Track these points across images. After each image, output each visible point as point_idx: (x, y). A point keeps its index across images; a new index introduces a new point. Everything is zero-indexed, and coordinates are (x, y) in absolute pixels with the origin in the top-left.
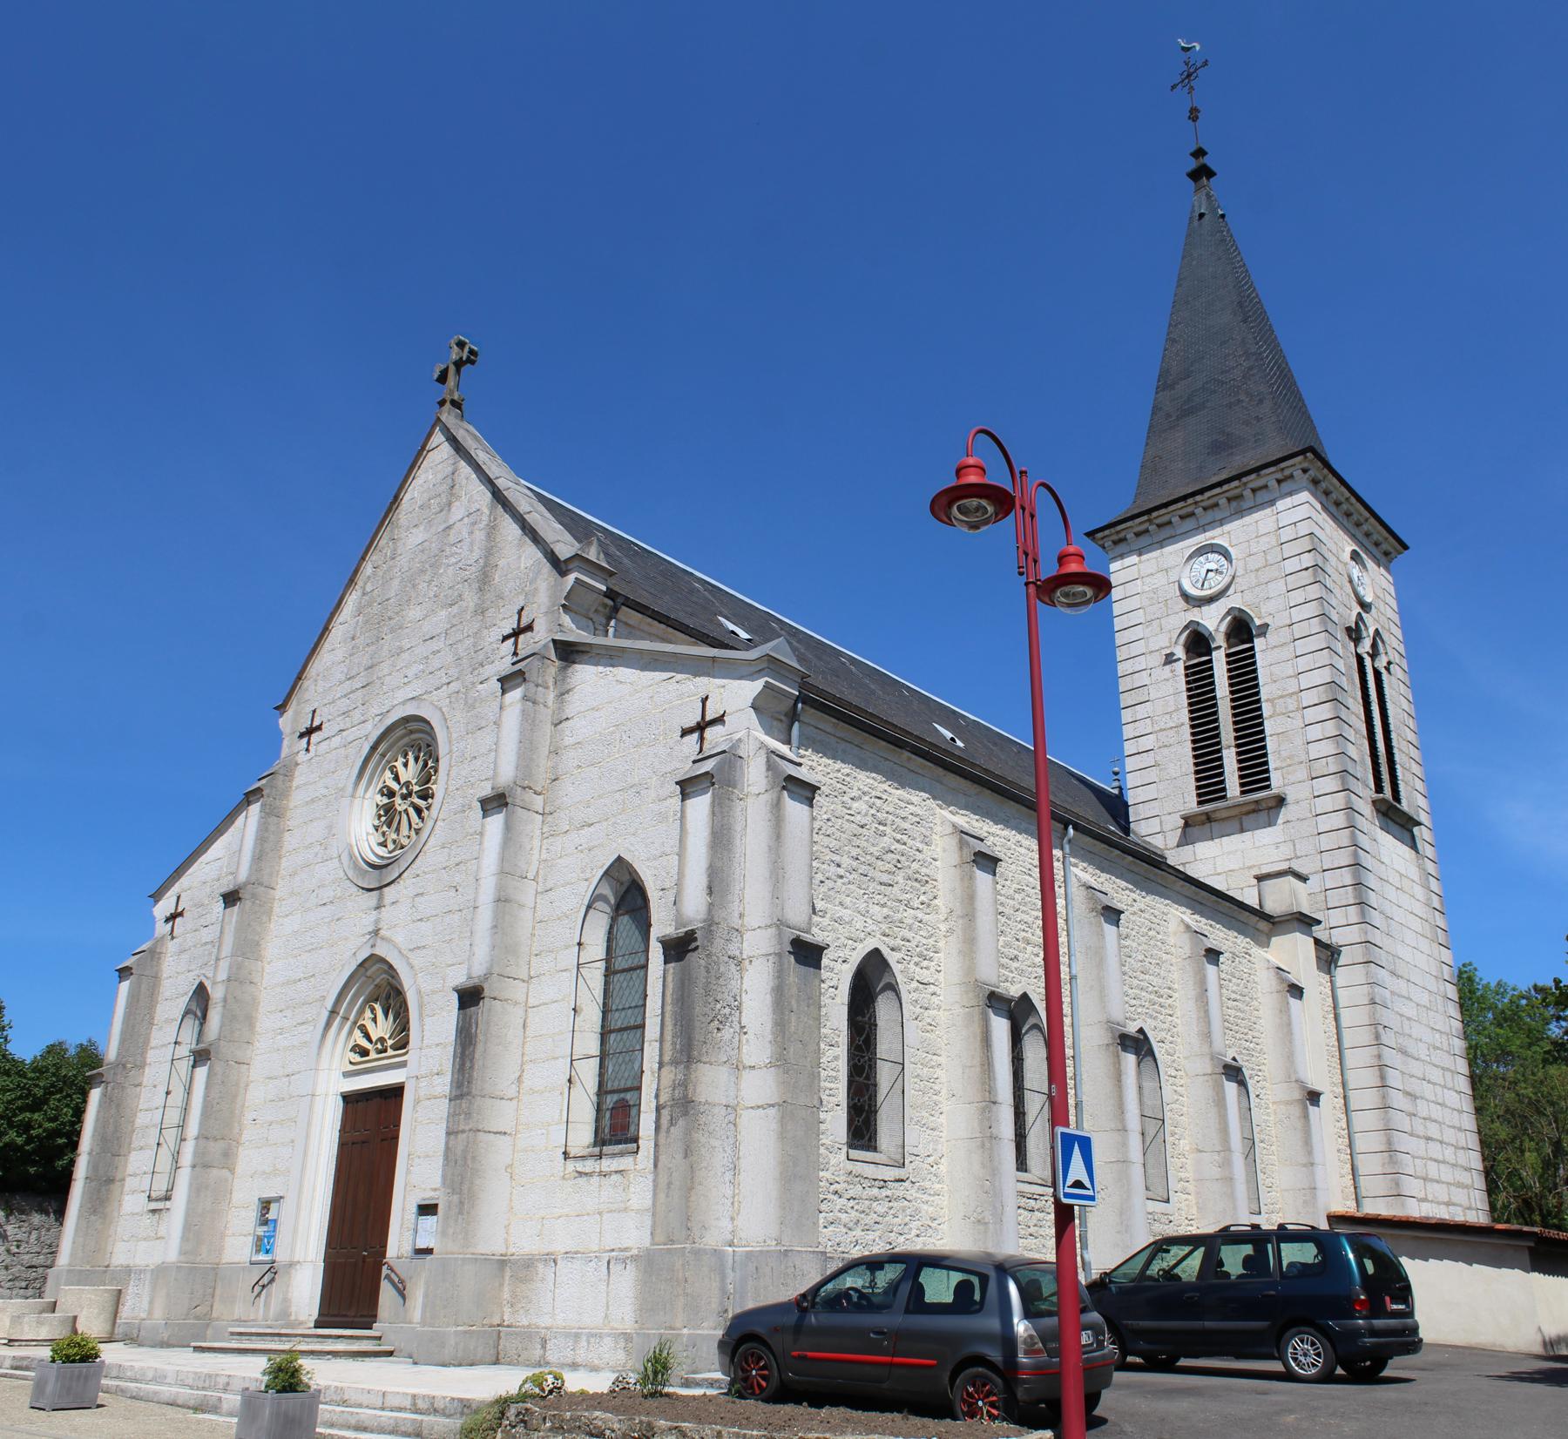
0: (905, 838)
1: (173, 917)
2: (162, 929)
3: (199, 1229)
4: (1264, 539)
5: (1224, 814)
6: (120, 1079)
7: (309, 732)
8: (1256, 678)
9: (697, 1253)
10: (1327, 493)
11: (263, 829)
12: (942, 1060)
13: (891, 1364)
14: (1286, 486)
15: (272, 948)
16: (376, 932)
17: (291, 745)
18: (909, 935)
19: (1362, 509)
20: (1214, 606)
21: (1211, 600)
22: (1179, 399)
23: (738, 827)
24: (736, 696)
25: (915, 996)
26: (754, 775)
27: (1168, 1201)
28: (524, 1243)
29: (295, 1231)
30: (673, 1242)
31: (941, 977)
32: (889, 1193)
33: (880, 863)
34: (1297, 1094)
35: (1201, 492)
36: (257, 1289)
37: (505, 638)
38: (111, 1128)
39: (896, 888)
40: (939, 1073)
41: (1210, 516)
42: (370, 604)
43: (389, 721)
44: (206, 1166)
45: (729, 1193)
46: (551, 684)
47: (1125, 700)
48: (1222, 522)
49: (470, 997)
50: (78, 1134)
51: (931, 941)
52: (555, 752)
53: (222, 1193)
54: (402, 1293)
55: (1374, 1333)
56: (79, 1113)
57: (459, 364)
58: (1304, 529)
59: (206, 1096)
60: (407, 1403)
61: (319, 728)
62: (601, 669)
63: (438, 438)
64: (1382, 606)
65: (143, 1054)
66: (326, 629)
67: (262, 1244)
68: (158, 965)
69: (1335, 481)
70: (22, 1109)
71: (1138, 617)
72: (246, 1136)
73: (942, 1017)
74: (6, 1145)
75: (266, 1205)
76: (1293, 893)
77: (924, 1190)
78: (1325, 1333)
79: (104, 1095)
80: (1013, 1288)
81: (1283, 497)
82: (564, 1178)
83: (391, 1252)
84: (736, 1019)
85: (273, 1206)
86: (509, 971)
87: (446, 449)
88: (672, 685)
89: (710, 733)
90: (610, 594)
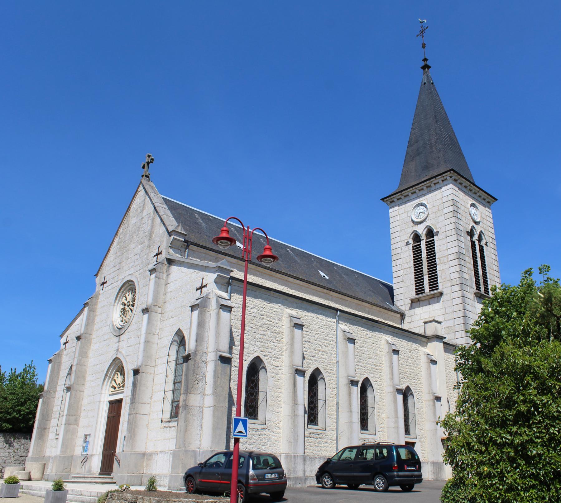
0: (271, 319)
1: (65, 343)
2: (63, 347)
3: (67, 444)
4: (438, 201)
5: (424, 299)
6: (48, 396)
7: (103, 284)
8: (434, 250)
9: (186, 451)
10: (461, 184)
11: (89, 315)
12: (282, 390)
13: (220, 483)
14: (445, 182)
15: (91, 354)
16: (118, 350)
17: (98, 288)
18: (271, 351)
19: (476, 188)
20: (422, 225)
21: (421, 223)
22: (416, 151)
24: (210, 278)
25: (272, 370)
26: (213, 304)
27: (375, 435)
28: (150, 448)
30: (180, 448)
31: (283, 364)
32: (259, 433)
34: (432, 398)
35: (417, 184)
36: (82, 463)
37: (155, 256)
40: (281, 394)
41: (421, 193)
42: (121, 242)
43: (124, 281)
44: (69, 424)
45: (199, 433)
46: (165, 272)
47: (394, 258)
48: (425, 195)
49: (136, 372)
50: (36, 413)
51: (280, 352)
52: (165, 294)
54: (119, 463)
55: (399, 476)
56: (36, 407)
57: (148, 163)
58: (450, 197)
59: (69, 402)
60: (96, 495)
61: (106, 283)
62: (178, 267)
63: (141, 188)
64: (485, 222)
65: (56, 388)
66: (109, 250)
67: (84, 449)
68: (61, 359)
69: (464, 180)
70: (18, 405)
71: (398, 229)
72: (83, 414)
73: (283, 376)
74: (13, 417)
75: (86, 436)
76: (435, 328)
77: (273, 432)
78: (385, 476)
79: (43, 401)
80: (251, 462)
81: (444, 186)
83: (117, 451)
84: (204, 380)
85: (88, 437)
87: (143, 192)
88: (195, 274)
89: (203, 289)
90: (185, 241)
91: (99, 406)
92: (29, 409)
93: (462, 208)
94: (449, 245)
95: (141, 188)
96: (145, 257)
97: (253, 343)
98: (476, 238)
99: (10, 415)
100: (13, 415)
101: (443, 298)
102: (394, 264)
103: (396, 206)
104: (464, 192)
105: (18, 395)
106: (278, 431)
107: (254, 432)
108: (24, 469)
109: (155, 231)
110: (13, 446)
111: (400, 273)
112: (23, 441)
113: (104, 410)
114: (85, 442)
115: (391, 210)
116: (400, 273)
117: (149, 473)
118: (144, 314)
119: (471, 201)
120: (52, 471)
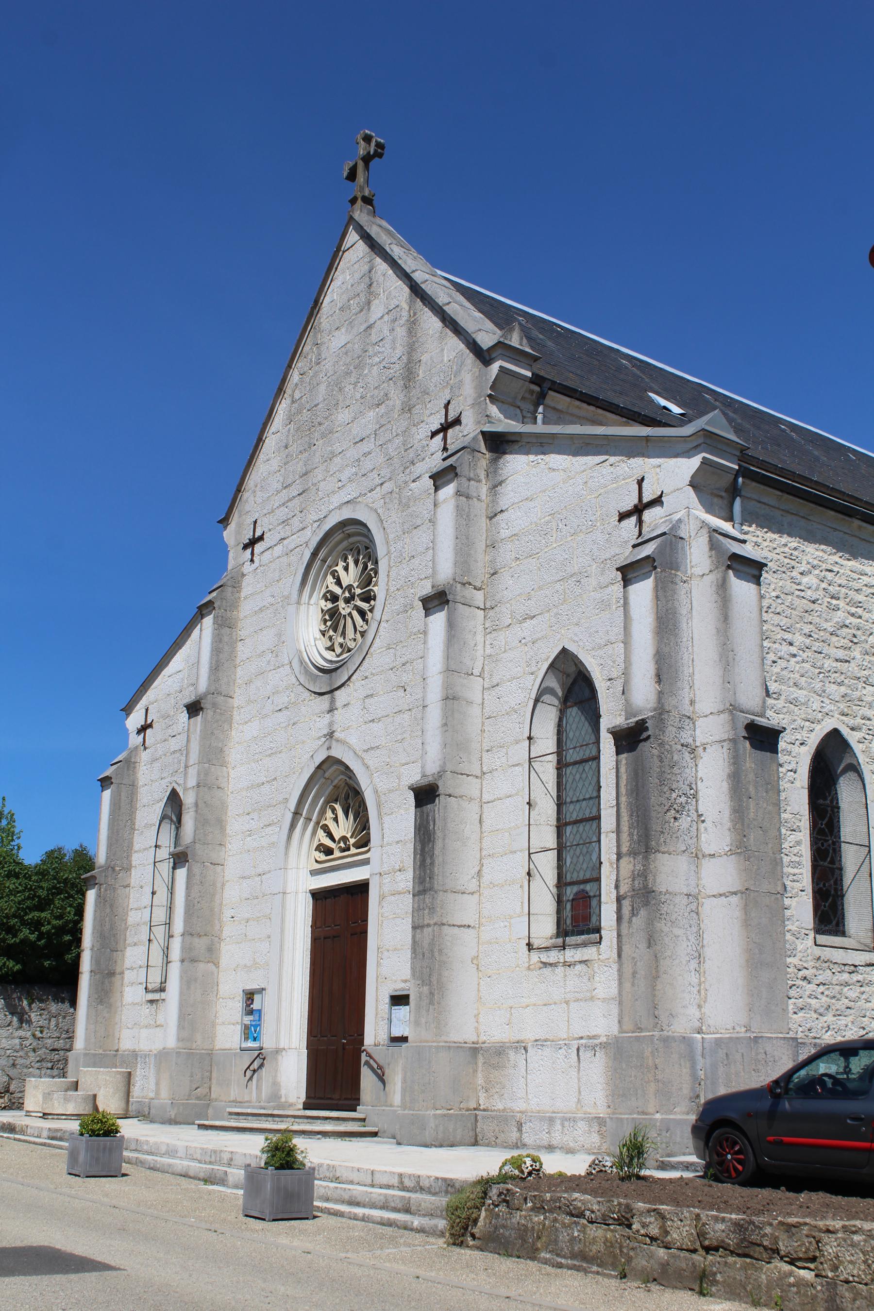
0: (860, 611)
1: (143, 729)
2: (135, 740)
6: (111, 881)
7: (252, 542)
9: (666, 1040)
15: (234, 754)
16: (331, 735)
17: (236, 557)
23: (684, 611)
26: (697, 556)
28: (494, 1032)
29: (278, 1020)
30: (641, 1030)
33: (834, 639)
36: (249, 1073)
37: (434, 434)
38: (108, 926)
39: (853, 664)
42: (299, 412)
44: (193, 960)
45: (695, 980)
46: (482, 476)
49: (425, 794)
50: (81, 931)
52: (492, 546)
53: (209, 986)
56: (80, 911)
57: (367, 159)
59: (188, 895)
60: (395, 1181)
61: (261, 538)
62: (532, 457)
63: (353, 236)
65: (129, 857)
66: (260, 440)
67: (250, 1032)
70: (31, 909)
72: (228, 931)
74: (22, 941)
75: (250, 996)
79: (99, 896)
82: (529, 968)
83: (369, 1039)
85: (257, 998)
87: (361, 247)
88: (606, 469)
90: (537, 380)
91: (283, 906)
92: (60, 917)
95: (353, 236)
96: (398, 441)
97: (818, 686)
99: (15, 936)
100: (21, 936)
105: (29, 878)
107: (845, 976)
109: (424, 358)
110: (29, 1022)
112: (54, 1007)
117: (500, 1106)
118: (428, 611)
120: (157, 1092)
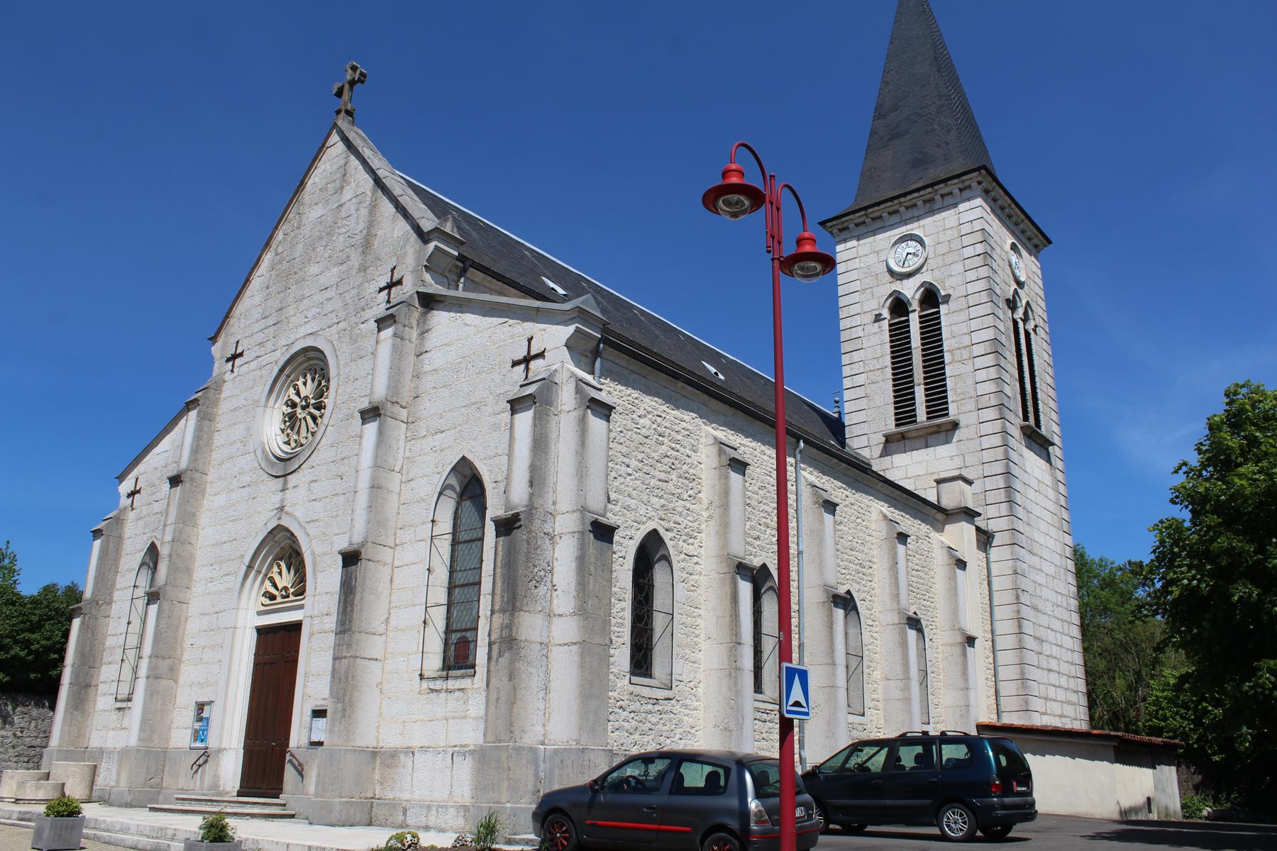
1: (132, 494)
2: (124, 502)
3: (153, 723)
4: (949, 232)
5: (914, 434)
6: (94, 612)
7: (234, 357)
9: (518, 749)
10: (995, 200)
14: (966, 194)
15: (204, 518)
16: (282, 508)
18: (679, 519)
20: (911, 280)
21: (909, 275)
22: (889, 126)
23: (553, 436)
25: (683, 564)
26: (566, 397)
28: (390, 739)
29: (222, 726)
30: (500, 741)
34: (959, 639)
36: (195, 767)
37: (381, 290)
39: (671, 484)
40: (699, 621)
41: (910, 213)
42: (280, 262)
44: (157, 677)
46: (415, 324)
47: (845, 347)
48: (918, 218)
49: (351, 558)
51: (696, 524)
54: (301, 773)
56: (66, 635)
57: (352, 83)
58: (978, 225)
59: (157, 626)
61: (241, 355)
63: (335, 138)
65: (111, 594)
66: (247, 281)
67: (198, 735)
68: (122, 528)
71: (856, 286)
73: (703, 580)
74: (13, 657)
75: (201, 707)
76: (962, 493)
77: (686, 706)
79: (83, 623)
81: (963, 201)
83: (293, 743)
84: (549, 580)
86: (380, 540)
87: (341, 147)
88: (506, 328)
90: (461, 258)
92: (48, 639)
93: (998, 249)
94: (974, 325)
96: (353, 292)
97: (645, 498)
98: (1019, 314)
100: (12, 652)
101: (958, 435)
102: (845, 359)
103: (851, 238)
104: (1000, 219)
106: (696, 704)
107: (650, 706)
108: (47, 776)
110: (12, 723)
111: (860, 380)
113: (246, 647)
114: (200, 719)
115: (839, 248)
116: (860, 380)
119: (1010, 240)
